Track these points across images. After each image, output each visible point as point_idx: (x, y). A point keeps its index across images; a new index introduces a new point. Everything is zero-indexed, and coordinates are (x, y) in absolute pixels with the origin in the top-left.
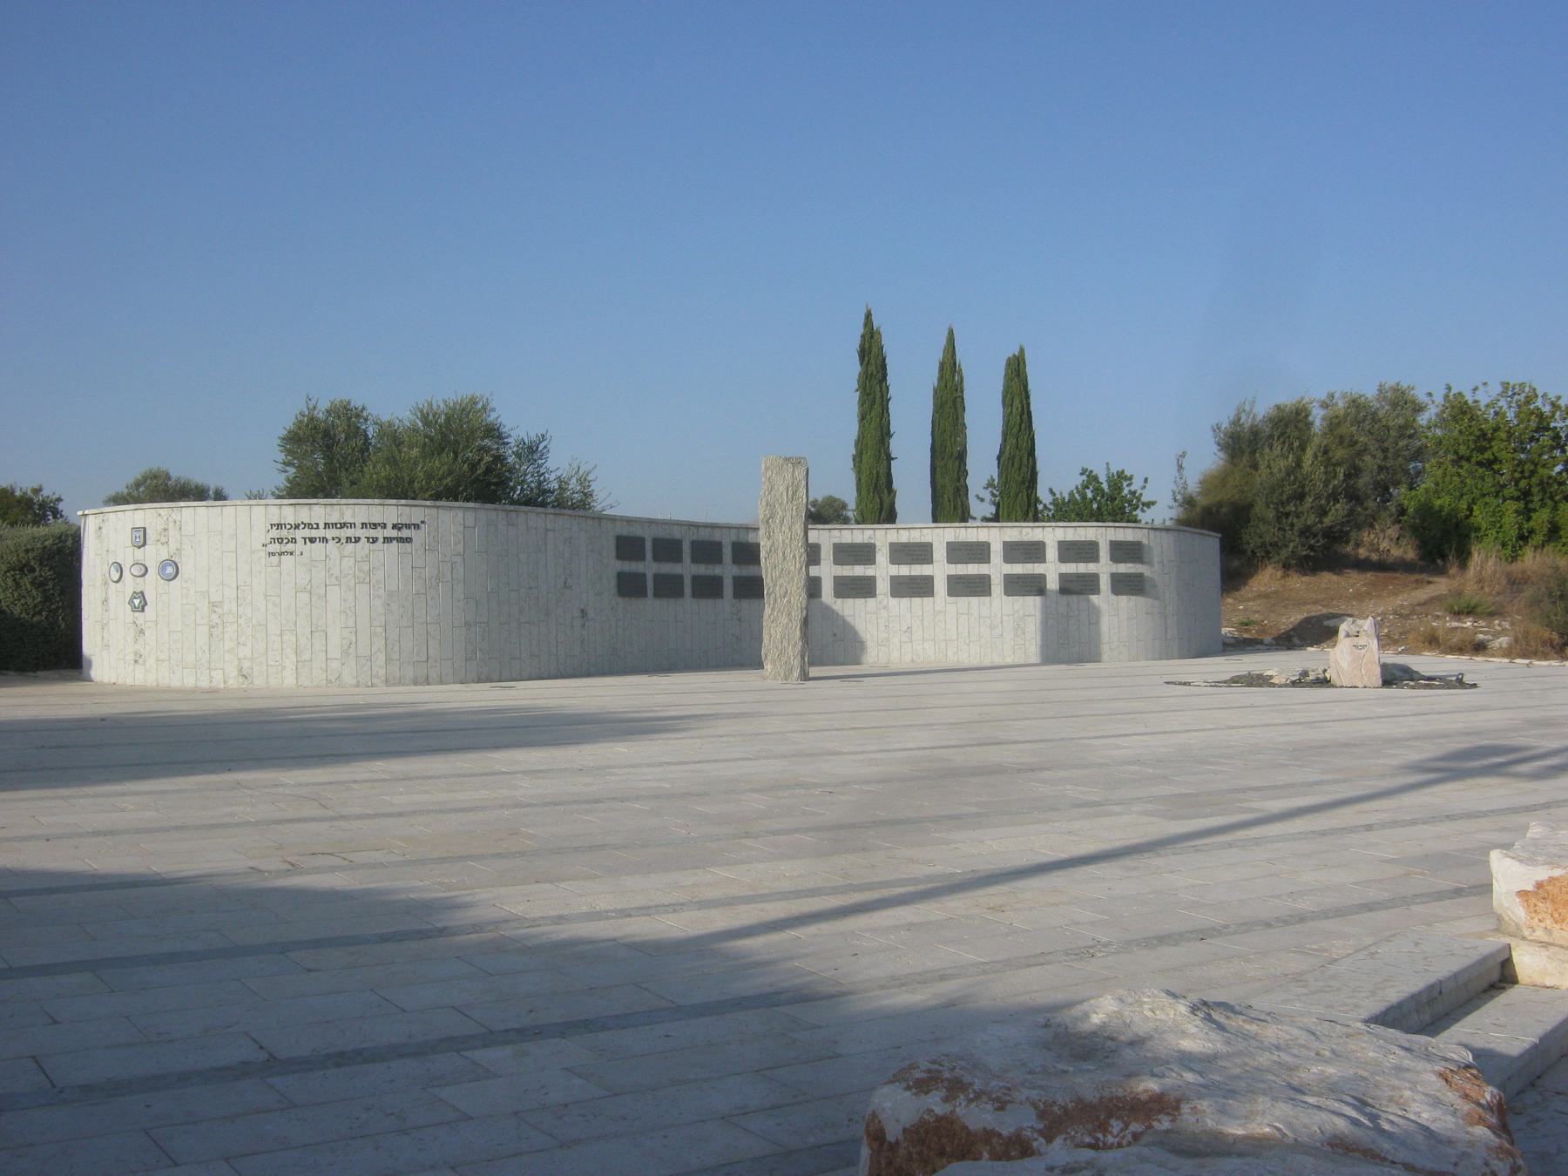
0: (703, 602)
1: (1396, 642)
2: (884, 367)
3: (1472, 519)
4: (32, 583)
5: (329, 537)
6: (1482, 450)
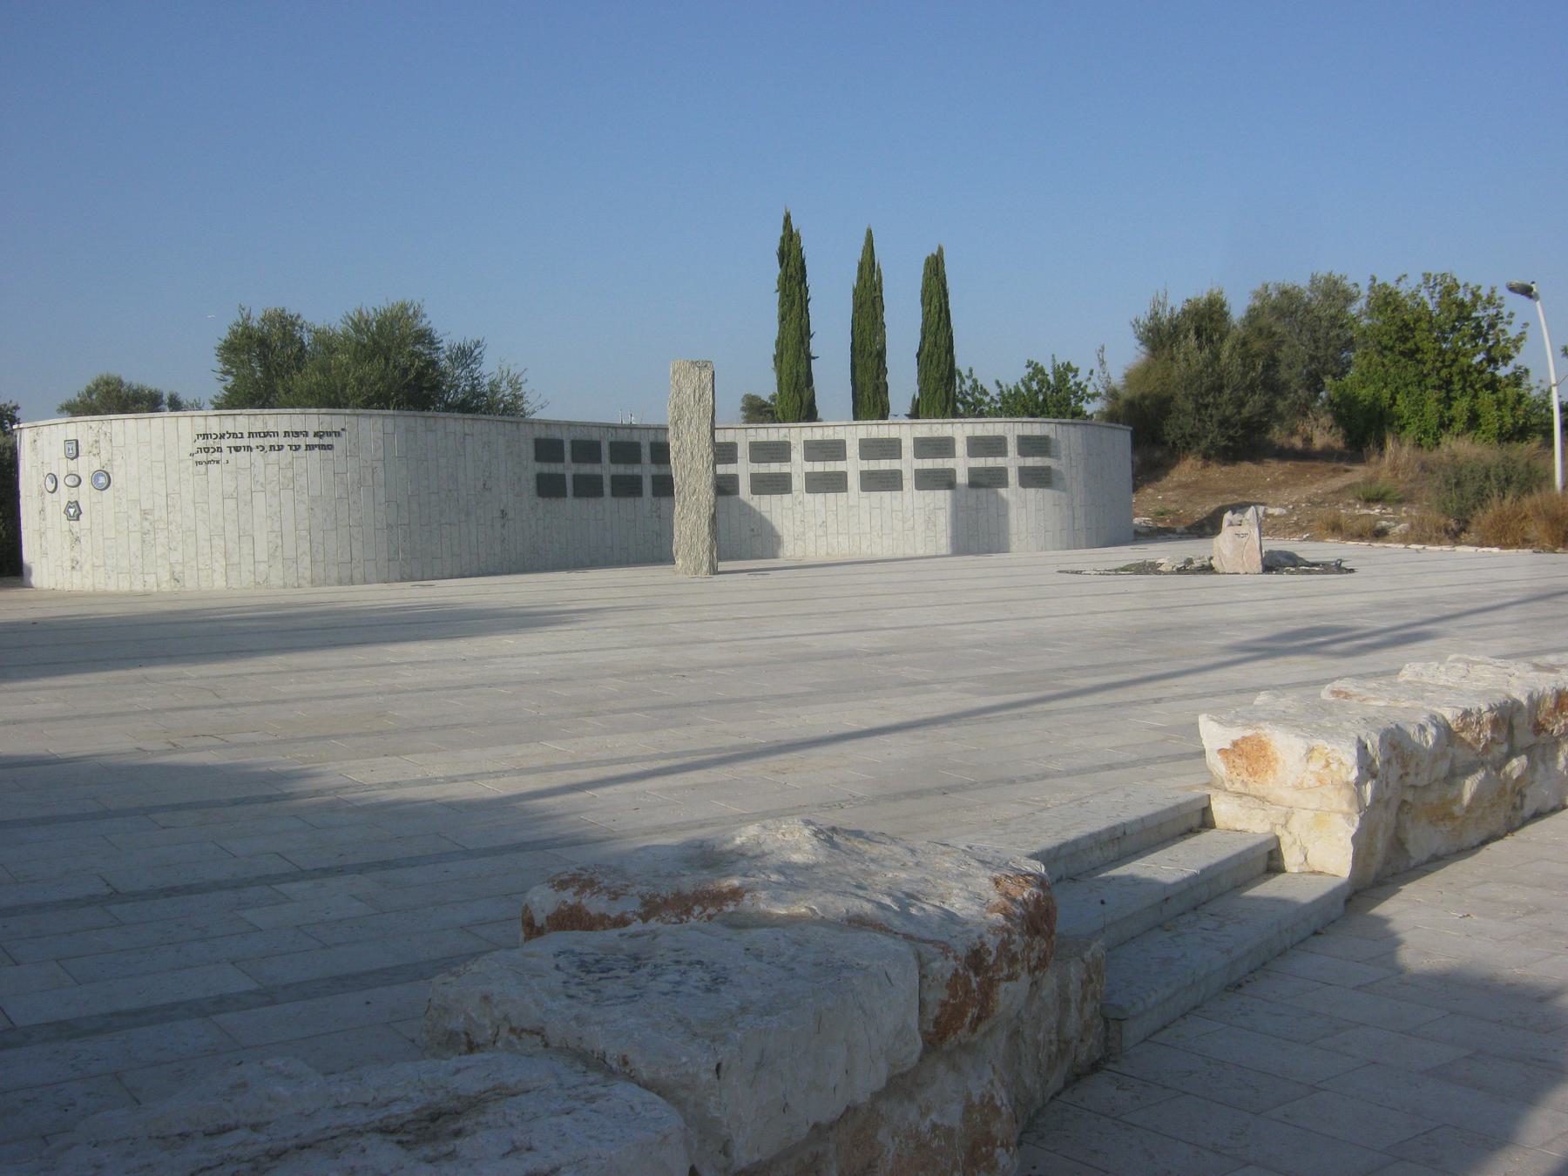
0: (623, 501)
1: (1303, 530)
2: (803, 268)
3: (1395, 408)
6: (1405, 340)
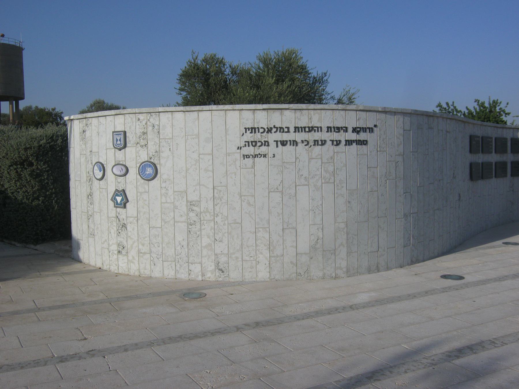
4: (31, 175)
5: (299, 140)
